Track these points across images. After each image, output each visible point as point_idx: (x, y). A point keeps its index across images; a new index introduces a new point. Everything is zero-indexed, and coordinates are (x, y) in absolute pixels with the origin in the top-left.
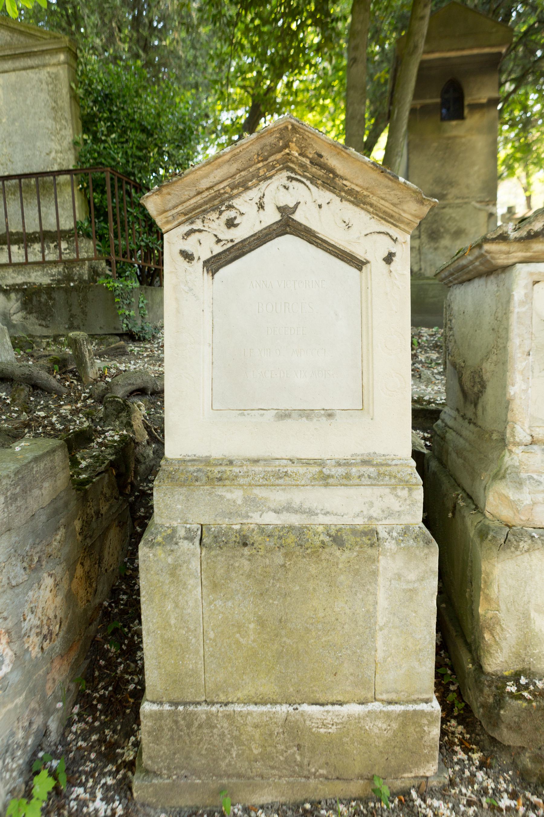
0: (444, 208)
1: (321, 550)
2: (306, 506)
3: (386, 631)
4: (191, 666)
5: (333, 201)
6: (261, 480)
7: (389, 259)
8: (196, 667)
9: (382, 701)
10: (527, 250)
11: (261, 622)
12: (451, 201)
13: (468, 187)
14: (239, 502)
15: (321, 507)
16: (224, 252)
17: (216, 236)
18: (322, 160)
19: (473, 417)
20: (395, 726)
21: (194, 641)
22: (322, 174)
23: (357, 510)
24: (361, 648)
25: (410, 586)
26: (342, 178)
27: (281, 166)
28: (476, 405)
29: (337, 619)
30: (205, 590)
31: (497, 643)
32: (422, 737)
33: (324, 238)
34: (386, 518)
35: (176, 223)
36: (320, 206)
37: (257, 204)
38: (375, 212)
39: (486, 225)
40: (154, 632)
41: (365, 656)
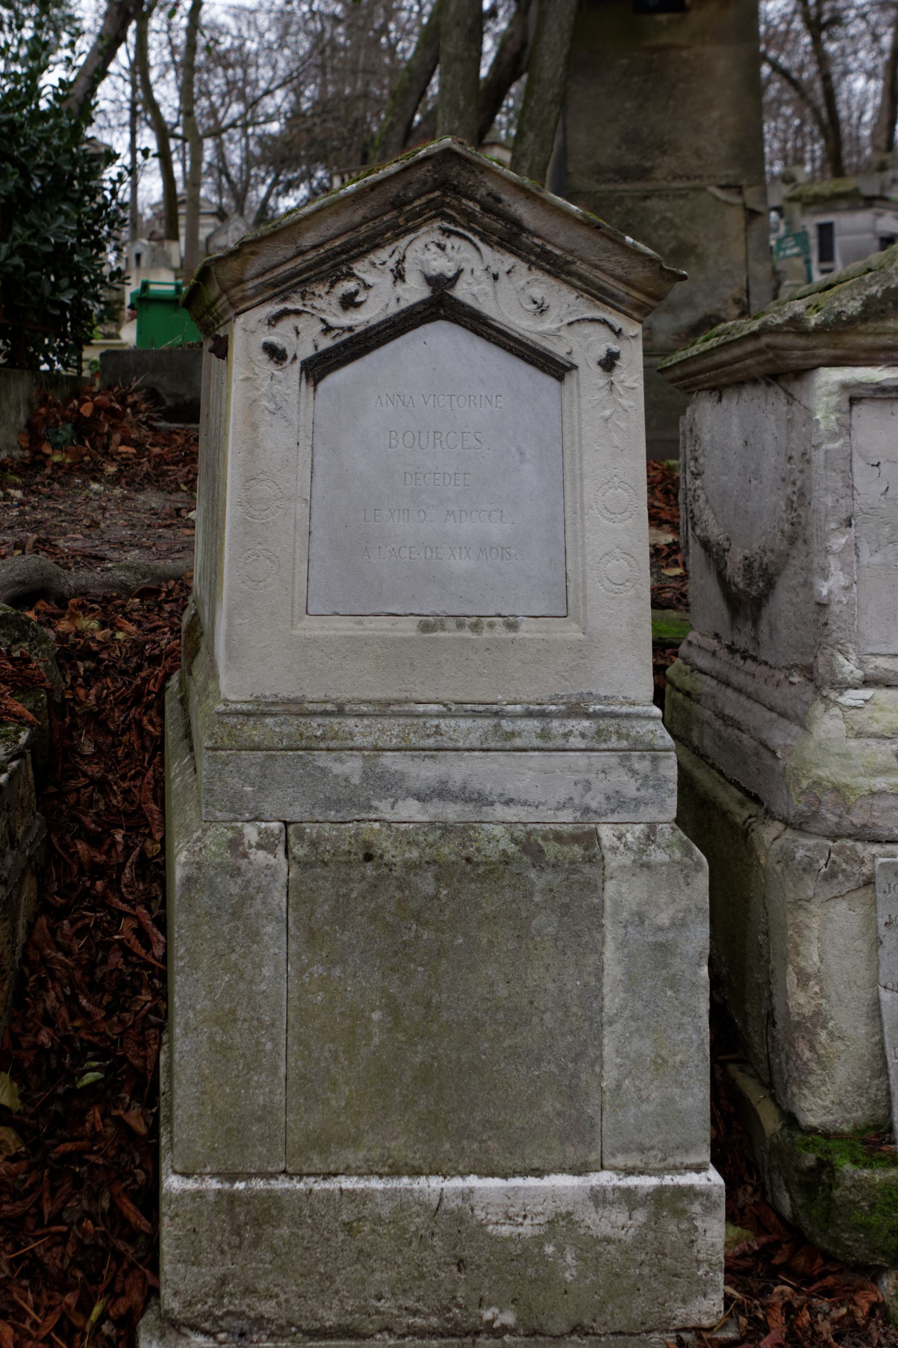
0: (646, 198)
1: (501, 867)
2: (475, 785)
3: (618, 1027)
4: (261, 1100)
5: (517, 268)
6: (394, 741)
7: (609, 362)
8: (272, 1101)
9: (614, 1169)
10: (835, 346)
11: (393, 1009)
12: (664, 184)
13: (698, 153)
14: (356, 780)
15: (499, 790)
16: (337, 347)
17: (323, 321)
18: (500, 206)
19: (750, 646)
20: (640, 1216)
21: (269, 1046)
22: (499, 226)
23: (562, 795)
24: (575, 1061)
25: (661, 937)
26: (529, 232)
27: (433, 212)
28: (755, 622)
29: (531, 1003)
30: (293, 947)
31: (819, 1060)
32: (692, 1242)
33: (502, 327)
34: (613, 811)
35: (259, 299)
36: (496, 277)
37: (392, 270)
38: (584, 287)
39: (742, 237)
40: (196, 1029)
41: (583, 1077)
